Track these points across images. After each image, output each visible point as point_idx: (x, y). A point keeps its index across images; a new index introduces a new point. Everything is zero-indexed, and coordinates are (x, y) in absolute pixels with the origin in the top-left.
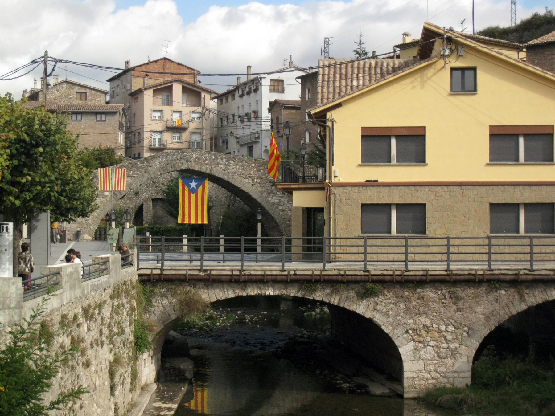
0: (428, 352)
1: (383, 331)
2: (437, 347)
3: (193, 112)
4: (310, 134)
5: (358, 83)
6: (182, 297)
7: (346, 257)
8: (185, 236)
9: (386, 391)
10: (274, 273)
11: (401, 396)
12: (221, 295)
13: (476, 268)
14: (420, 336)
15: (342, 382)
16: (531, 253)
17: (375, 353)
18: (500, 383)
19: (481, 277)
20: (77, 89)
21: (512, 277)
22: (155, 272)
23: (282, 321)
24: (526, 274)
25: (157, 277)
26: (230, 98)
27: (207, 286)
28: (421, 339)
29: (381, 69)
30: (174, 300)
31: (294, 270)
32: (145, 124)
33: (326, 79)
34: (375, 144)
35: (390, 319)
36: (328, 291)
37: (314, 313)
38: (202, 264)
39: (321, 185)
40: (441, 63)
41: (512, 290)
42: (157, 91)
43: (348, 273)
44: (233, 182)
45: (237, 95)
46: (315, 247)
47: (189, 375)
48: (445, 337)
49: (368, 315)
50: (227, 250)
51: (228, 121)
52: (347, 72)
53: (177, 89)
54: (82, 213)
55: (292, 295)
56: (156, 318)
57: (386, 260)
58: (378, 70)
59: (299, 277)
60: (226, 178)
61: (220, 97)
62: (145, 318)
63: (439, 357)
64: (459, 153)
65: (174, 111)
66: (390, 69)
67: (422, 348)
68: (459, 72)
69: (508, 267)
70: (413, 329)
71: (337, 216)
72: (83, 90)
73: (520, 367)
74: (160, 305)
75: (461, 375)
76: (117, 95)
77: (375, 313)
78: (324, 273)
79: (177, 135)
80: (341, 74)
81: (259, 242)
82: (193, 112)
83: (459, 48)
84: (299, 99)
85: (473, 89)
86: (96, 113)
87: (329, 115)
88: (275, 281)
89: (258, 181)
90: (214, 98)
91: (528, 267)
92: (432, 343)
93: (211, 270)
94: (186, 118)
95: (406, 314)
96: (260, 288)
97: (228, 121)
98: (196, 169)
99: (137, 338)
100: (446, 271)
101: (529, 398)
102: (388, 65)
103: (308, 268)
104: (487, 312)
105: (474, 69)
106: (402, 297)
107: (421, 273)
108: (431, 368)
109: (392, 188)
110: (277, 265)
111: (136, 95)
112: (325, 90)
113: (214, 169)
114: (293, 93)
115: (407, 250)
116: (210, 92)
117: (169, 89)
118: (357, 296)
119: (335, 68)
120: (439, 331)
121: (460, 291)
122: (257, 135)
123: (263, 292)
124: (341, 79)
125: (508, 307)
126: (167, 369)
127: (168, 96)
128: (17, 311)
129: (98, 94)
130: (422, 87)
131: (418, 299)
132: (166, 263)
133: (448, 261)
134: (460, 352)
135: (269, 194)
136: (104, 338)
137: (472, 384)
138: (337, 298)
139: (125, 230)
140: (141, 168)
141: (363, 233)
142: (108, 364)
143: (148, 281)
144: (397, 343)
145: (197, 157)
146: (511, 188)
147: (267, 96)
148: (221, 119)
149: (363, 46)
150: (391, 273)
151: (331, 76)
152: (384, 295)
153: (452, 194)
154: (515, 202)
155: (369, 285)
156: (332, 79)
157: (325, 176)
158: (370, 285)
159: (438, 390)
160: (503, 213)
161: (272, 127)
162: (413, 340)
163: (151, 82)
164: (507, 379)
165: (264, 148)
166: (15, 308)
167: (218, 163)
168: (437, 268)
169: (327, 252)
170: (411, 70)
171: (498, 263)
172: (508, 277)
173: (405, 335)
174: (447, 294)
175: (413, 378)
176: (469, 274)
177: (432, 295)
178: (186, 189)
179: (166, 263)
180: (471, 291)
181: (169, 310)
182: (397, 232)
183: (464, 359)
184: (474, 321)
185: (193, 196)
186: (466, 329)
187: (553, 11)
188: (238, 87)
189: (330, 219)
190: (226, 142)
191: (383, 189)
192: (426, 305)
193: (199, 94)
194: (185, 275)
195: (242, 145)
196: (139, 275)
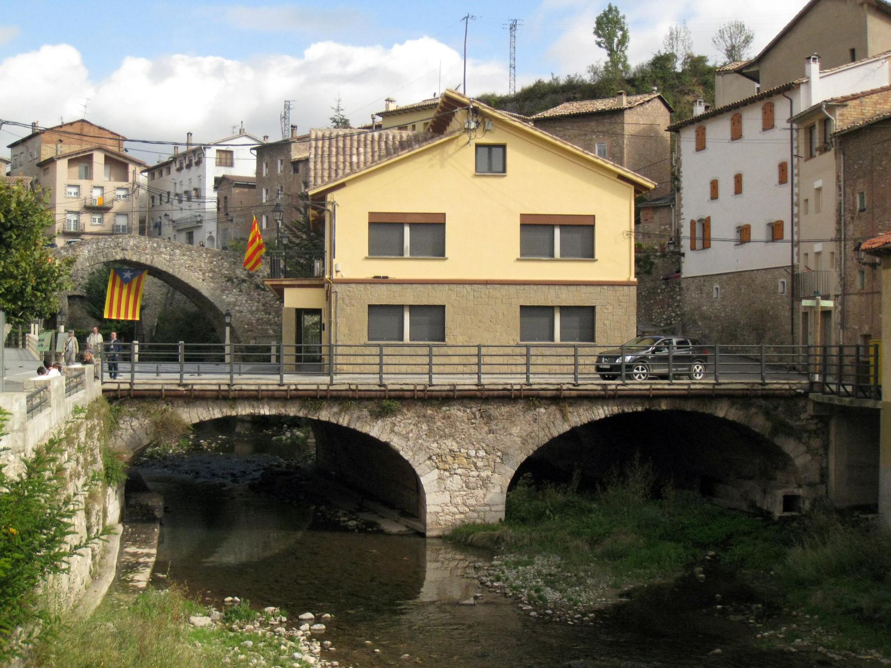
0: (455, 482)
1: (401, 457)
2: (465, 475)
3: (118, 188)
4: (267, 218)
5: (359, 159)
6: (158, 418)
7: (350, 368)
9: (404, 529)
10: (271, 387)
11: (423, 535)
12: (205, 415)
13: (512, 381)
14: (445, 462)
15: (346, 519)
16: (576, 364)
17: (389, 484)
18: (539, 516)
19: (517, 392)
21: (554, 392)
23: (238, 447)
24: (570, 390)
25: (126, 393)
26: (164, 172)
27: (188, 404)
28: (447, 466)
29: (386, 143)
30: (147, 421)
31: (296, 385)
32: (57, 201)
33: (320, 152)
34: (385, 232)
35: (411, 443)
36: (335, 409)
37: (284, 438)
38: (181, 376)
39: (320, 283)
40: (465, 138)
41: (553, 408)
42: (74, 161)
43: (360, 387)
44: (179, 276)
45: (174, 168)
46: (310, 357)
47: (158, 514)
48: (475, 464)
49: (383, 438)
50: (188, 359)
51: (161, 200)
52: (344, 145)
53: (99, 158)
54: (40, 313)
55: (292, 414)
56: (123, 444)
57: (405, 371)
58: (383, 144)
59: (300, 393)
60: (171, 271)
61: (151, 171)
62: (110, 444)
63: (467, 487)
64: (483, 246)
65: (95, 187)
66: (397, 143)
67: (447, 477)
68: (486, 150)
70: (438, 455)
71: (338, 320)
73: (560, 498)
74: (129, 427)
75: (494, 508)
76: (21, 165)
77: (392, 436)
78: (331, 388)
79: (97, 217)
80: (337, 148)
81: (227, 350)
82: (118, 188)
83: (487, 120)
84: (255, 176)
85: (501, 170)
87: (330, 197)
88: (271, 397)
89: (211, 275)
92: (459, 471)
93: (193, 384)
94: (109, 196)
95: (429, 437)
96: (253, 407)
97: (161, 200)
98: (134, 260)
99: (107, 468)
100: (477, 385)
101: (576, 534)
102: (394, 138)
103: (312, 382)
105: (503, 147)
106: (424, 416)
107: (448, 388)
108: (459, 500)
109: (405, 286)
110: (224, 379)
112: (319, 166)
113: (156, 260)
114: (246, 166)
116: (139, 164)
118: (371, 415)
119: (351, 140)
120: (468, 457)
121: (494, 410)
122: (199, 219)
123: (257, 411)
124: (337, 154)
125: (549, 428)
126: (131, 506)
127: (86, 168)
128: (21, 434)
130: (442, 166)
131: (443, 418)
132: (137, 375)
133: (479, 373)
134: (493, 481)
135: (223, 291)
136: (80, 468)
137: (506, 519)
138: (347, 418)
139: (59, 335)
141: (369, 339)
143: (113, 397)
144: (418, 472)
145: (135, 245)
146: (545, 288)
147: (212, 170)
148: (153, 198)
149: (341, 113)
150: (412, 387)
151: (326, 149)
152: (403, 414)
153: (476, 294)
154: (550, 304)
155: (385, 403)
156: (326, 154)
157: (324, 271)
158: (385, 402)
159: (466, 526)
160: (535, 317)
161: (218, 209)
162: (438, 468)
163: (65, 149)
164: (548, 512)
165: (207, 235)
166: (18, 430)
167: (162, 253)
168: (467, 382)
169: (326, 362)
170: (429, 146)
171: (465, 376)
172: (549, 392)
173: (428, 462)
174: (477, 413)
175: (438, 513)
176: (504, 389)
177: (460, 414)
179: (137, 375)
180: (505, 410)
181: (141, 433)
182: (411, 340)
183: (497, 489)
184: (509, 444)
186: (499, 454)
188: (174, 159)
189: (330, 323)
190: (158, 226)
191: (394, 287)
192: (453, 426)
193: (125, 166)
194: (160, 390)
195: (179, 231)
196: (104, 391)
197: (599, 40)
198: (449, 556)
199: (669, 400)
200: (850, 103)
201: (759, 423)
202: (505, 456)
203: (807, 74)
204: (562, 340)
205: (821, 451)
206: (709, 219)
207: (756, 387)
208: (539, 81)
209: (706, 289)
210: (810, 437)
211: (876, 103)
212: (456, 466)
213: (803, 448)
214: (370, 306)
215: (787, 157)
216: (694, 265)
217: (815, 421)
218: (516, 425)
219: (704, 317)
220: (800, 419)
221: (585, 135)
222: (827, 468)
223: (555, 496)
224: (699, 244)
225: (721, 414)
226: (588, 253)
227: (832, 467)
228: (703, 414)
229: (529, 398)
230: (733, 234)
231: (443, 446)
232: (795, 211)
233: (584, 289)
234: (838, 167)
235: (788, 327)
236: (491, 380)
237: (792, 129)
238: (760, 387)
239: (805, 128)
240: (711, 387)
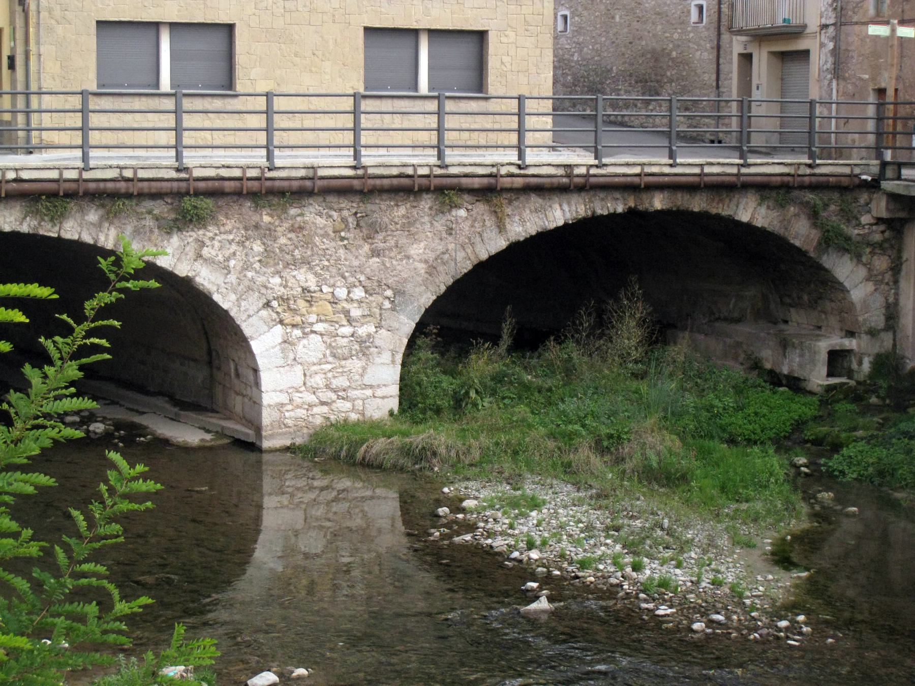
0: (312, 348)
28: (298, 319)
35: (232, 278)
41: (481, 208)
43: (142, 174)
48: (347, 313)
70: (283, 299)
75: (379, 393)
78: (86, 175)
91: (433, 160)
104: (431, 256)
106: (257, 227)
107: (302, 173)
108: (318, 380)
131: (292, 230)
138: (113, 232)
144: (247, 330)
150: (237, 173)
173: (264, 313)
176: (399, 176)
186: (389, 293)
192: (308, 243)
201: (801, 232)
205: (888, 277)
210: (872, 253)
212: (313, 318)
213: (862, 272)
220: (859, 225)
236: (292, 162)
240: (734, 170)
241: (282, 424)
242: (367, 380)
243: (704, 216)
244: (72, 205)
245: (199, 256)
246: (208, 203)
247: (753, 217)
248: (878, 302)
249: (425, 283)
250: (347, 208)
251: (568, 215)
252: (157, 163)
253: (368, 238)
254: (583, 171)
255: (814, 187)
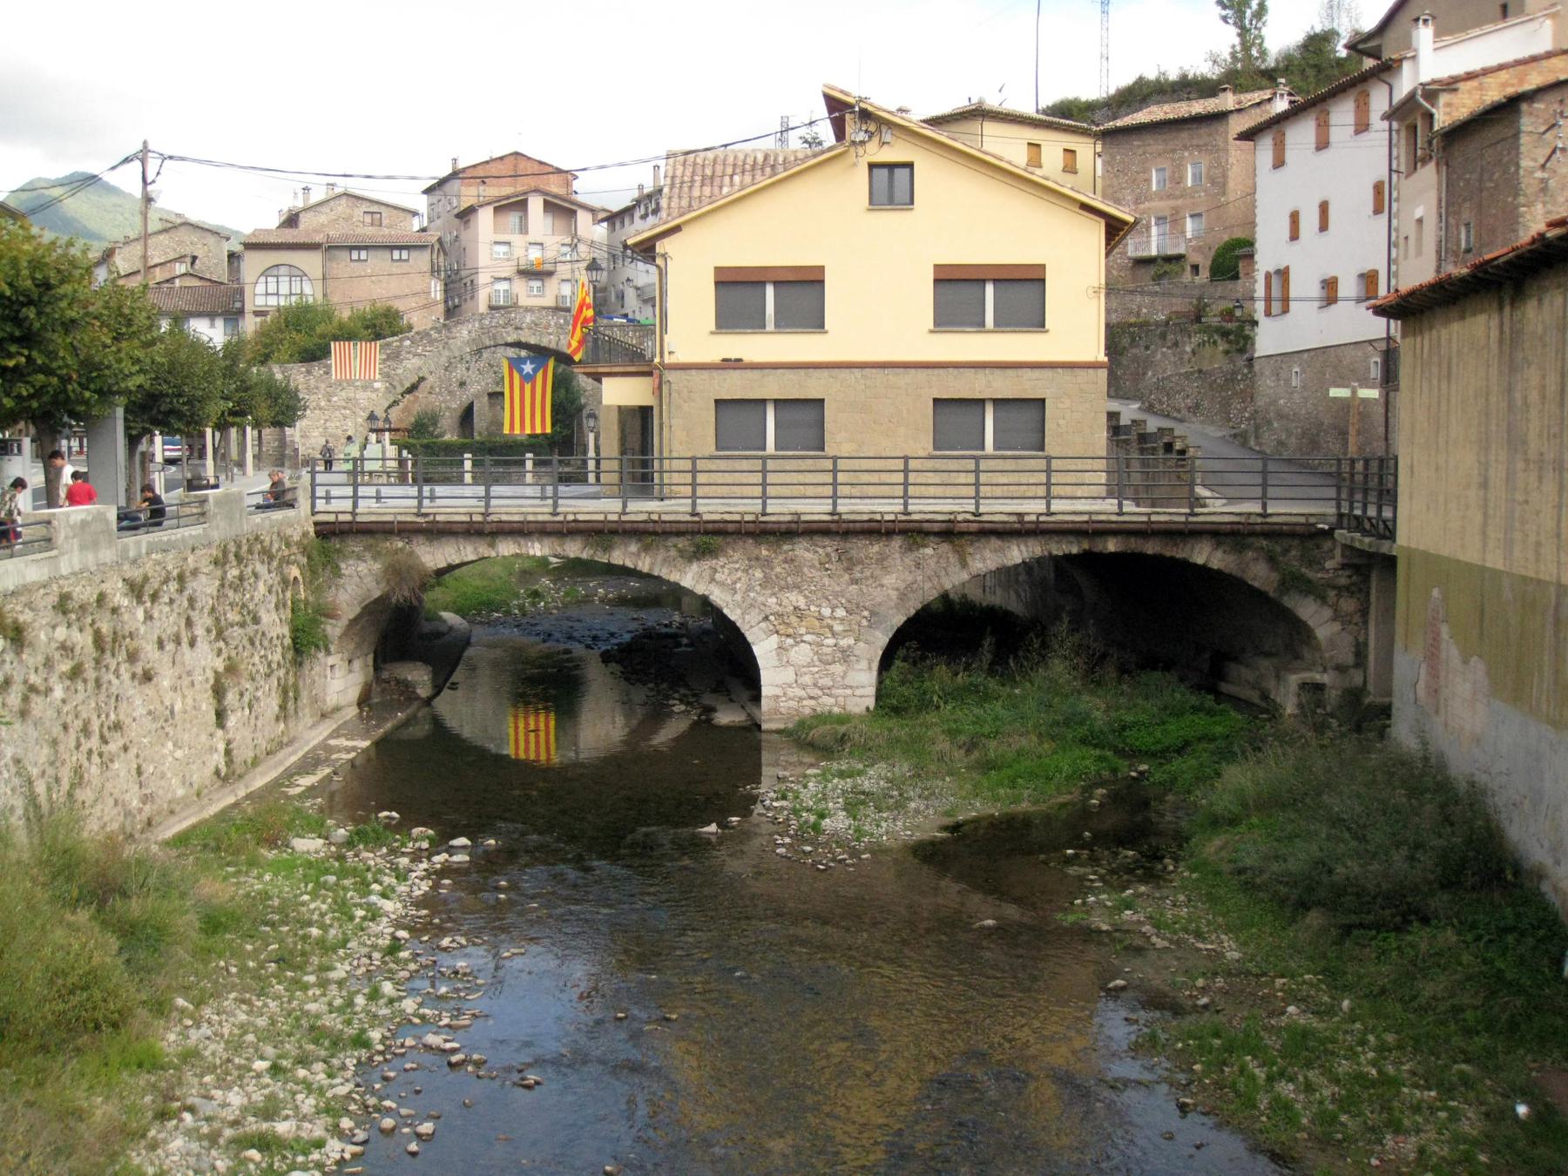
0: (802, 653)
8: (467, 456)
20: (365, 207)
22: (342, 518)
25: (346, 527)
26: (627, 221)
28: (790, 631)
34: (739, 295)
35: (738, 597)
41: (945, 547)
43: (665, 517)
45: (637, 214)
46: (640, 471)
48: (830, 628)
49: (700, 589)
53: (536, 204)
64: (880, 314)
68: (885, 172)
69: (937, 508)
70: (779, 615)
72: (375, 208)
75: (858, 692)
78: (624, 518)
79: (536, 284)
83: (884, 129)
86: (392, 248)
90: (603, 220)
91: (972, 508)
92: (808, 638)
104: (902, 586)
106: (757, 559)
107: (789, 518)
108: (807, 679)
111: (466, 215)
115: (977, 478)
117: (521, 205)
129: (401, 214)
131: (785, 561)
133: (835, 497)
138: (648, 560)
140: (436, 340)
141: (717, 449)
142: (210, 675)
144: (750, 638)
150: (737, 517)
158: (707, 538)
160: (955, 416)
164: (935, 698)
169: (656, 481)
173: (763, 625)
176: (870, 521)
177: (808, 555)
178: (516, 376)
182: (777, 449)
185: (528, 387)
186: (866, 613)
187: (1186, 67)
188: (638, 202)
191: (749, 374)
192: (798, 571)
193: (574, 212)
196: (316, 524)
197: (1224, 13)
198: (794, 759)
199: (1119, 538)
200: (1462, 86)
201: (1259, 574)
202: (875, 616)
203: (1414, 45)
204: (996, 448)
205: (1357, 618)
206: (1287, 268)
207: (1252, 520)
208: (1141, 78)
209: (1283, 375)
210: (1339, 596)
211: (1505, 85)
212: (803, 631)
213: (1327, 613)
214: (717, 401)
215: (1383, 173)
216: (1270, 338)
217: (1348, 573)
218: (889, 573)
219: (1281, 416)
220: (1323, 569)
221: (1174, 151)
222: (1366, 644)
223: (941, 675)
224: (1276, 307)
225: (1200, 560)
226: (1036, 321)
227: (1372, 644)
228: (1172, 558)
229: (912, 533)
230: (1315, 291)
231: (785, 602)
232: (1394, 255)
233: (1028, 373)
234: (1440, 183)
235: (1381, 430)
236: (854, 508)
237: (1390, 130)
238: (1259, 520)
239: (1408, 127)
240: (1183, 519)
241: (777, 711)
242: (847, 681)
243: (1158, 558)
244: (616, 539)
245: (713, 580)
246: (719, 540)
247: (1208, 559)
248: (1347, 641)
249: (897, 606)
250: (829, 546)
251: (1025, 555)
252: (745, 508)
253: (848, 569)
254: (1033, 518)
255: (1267, 535)
